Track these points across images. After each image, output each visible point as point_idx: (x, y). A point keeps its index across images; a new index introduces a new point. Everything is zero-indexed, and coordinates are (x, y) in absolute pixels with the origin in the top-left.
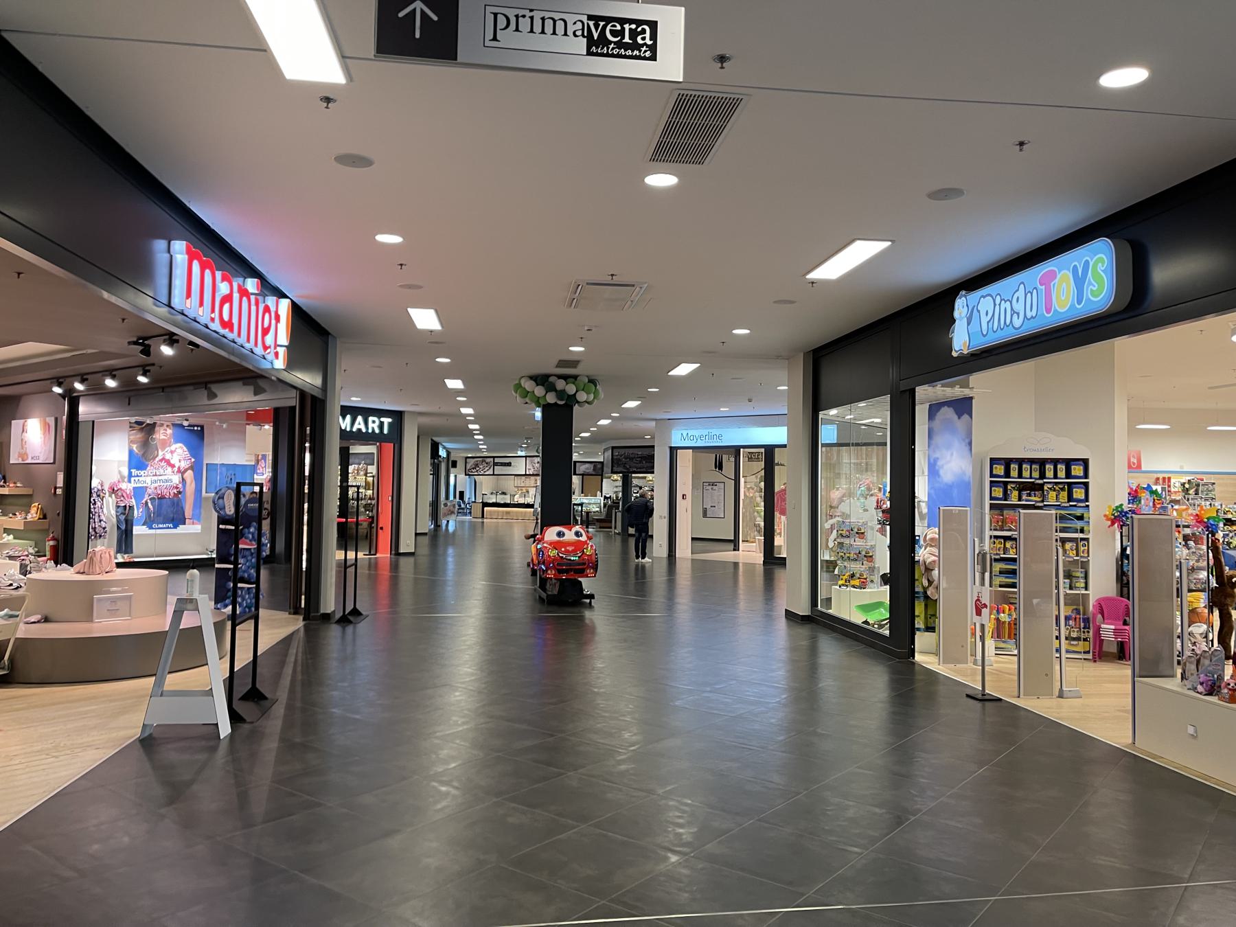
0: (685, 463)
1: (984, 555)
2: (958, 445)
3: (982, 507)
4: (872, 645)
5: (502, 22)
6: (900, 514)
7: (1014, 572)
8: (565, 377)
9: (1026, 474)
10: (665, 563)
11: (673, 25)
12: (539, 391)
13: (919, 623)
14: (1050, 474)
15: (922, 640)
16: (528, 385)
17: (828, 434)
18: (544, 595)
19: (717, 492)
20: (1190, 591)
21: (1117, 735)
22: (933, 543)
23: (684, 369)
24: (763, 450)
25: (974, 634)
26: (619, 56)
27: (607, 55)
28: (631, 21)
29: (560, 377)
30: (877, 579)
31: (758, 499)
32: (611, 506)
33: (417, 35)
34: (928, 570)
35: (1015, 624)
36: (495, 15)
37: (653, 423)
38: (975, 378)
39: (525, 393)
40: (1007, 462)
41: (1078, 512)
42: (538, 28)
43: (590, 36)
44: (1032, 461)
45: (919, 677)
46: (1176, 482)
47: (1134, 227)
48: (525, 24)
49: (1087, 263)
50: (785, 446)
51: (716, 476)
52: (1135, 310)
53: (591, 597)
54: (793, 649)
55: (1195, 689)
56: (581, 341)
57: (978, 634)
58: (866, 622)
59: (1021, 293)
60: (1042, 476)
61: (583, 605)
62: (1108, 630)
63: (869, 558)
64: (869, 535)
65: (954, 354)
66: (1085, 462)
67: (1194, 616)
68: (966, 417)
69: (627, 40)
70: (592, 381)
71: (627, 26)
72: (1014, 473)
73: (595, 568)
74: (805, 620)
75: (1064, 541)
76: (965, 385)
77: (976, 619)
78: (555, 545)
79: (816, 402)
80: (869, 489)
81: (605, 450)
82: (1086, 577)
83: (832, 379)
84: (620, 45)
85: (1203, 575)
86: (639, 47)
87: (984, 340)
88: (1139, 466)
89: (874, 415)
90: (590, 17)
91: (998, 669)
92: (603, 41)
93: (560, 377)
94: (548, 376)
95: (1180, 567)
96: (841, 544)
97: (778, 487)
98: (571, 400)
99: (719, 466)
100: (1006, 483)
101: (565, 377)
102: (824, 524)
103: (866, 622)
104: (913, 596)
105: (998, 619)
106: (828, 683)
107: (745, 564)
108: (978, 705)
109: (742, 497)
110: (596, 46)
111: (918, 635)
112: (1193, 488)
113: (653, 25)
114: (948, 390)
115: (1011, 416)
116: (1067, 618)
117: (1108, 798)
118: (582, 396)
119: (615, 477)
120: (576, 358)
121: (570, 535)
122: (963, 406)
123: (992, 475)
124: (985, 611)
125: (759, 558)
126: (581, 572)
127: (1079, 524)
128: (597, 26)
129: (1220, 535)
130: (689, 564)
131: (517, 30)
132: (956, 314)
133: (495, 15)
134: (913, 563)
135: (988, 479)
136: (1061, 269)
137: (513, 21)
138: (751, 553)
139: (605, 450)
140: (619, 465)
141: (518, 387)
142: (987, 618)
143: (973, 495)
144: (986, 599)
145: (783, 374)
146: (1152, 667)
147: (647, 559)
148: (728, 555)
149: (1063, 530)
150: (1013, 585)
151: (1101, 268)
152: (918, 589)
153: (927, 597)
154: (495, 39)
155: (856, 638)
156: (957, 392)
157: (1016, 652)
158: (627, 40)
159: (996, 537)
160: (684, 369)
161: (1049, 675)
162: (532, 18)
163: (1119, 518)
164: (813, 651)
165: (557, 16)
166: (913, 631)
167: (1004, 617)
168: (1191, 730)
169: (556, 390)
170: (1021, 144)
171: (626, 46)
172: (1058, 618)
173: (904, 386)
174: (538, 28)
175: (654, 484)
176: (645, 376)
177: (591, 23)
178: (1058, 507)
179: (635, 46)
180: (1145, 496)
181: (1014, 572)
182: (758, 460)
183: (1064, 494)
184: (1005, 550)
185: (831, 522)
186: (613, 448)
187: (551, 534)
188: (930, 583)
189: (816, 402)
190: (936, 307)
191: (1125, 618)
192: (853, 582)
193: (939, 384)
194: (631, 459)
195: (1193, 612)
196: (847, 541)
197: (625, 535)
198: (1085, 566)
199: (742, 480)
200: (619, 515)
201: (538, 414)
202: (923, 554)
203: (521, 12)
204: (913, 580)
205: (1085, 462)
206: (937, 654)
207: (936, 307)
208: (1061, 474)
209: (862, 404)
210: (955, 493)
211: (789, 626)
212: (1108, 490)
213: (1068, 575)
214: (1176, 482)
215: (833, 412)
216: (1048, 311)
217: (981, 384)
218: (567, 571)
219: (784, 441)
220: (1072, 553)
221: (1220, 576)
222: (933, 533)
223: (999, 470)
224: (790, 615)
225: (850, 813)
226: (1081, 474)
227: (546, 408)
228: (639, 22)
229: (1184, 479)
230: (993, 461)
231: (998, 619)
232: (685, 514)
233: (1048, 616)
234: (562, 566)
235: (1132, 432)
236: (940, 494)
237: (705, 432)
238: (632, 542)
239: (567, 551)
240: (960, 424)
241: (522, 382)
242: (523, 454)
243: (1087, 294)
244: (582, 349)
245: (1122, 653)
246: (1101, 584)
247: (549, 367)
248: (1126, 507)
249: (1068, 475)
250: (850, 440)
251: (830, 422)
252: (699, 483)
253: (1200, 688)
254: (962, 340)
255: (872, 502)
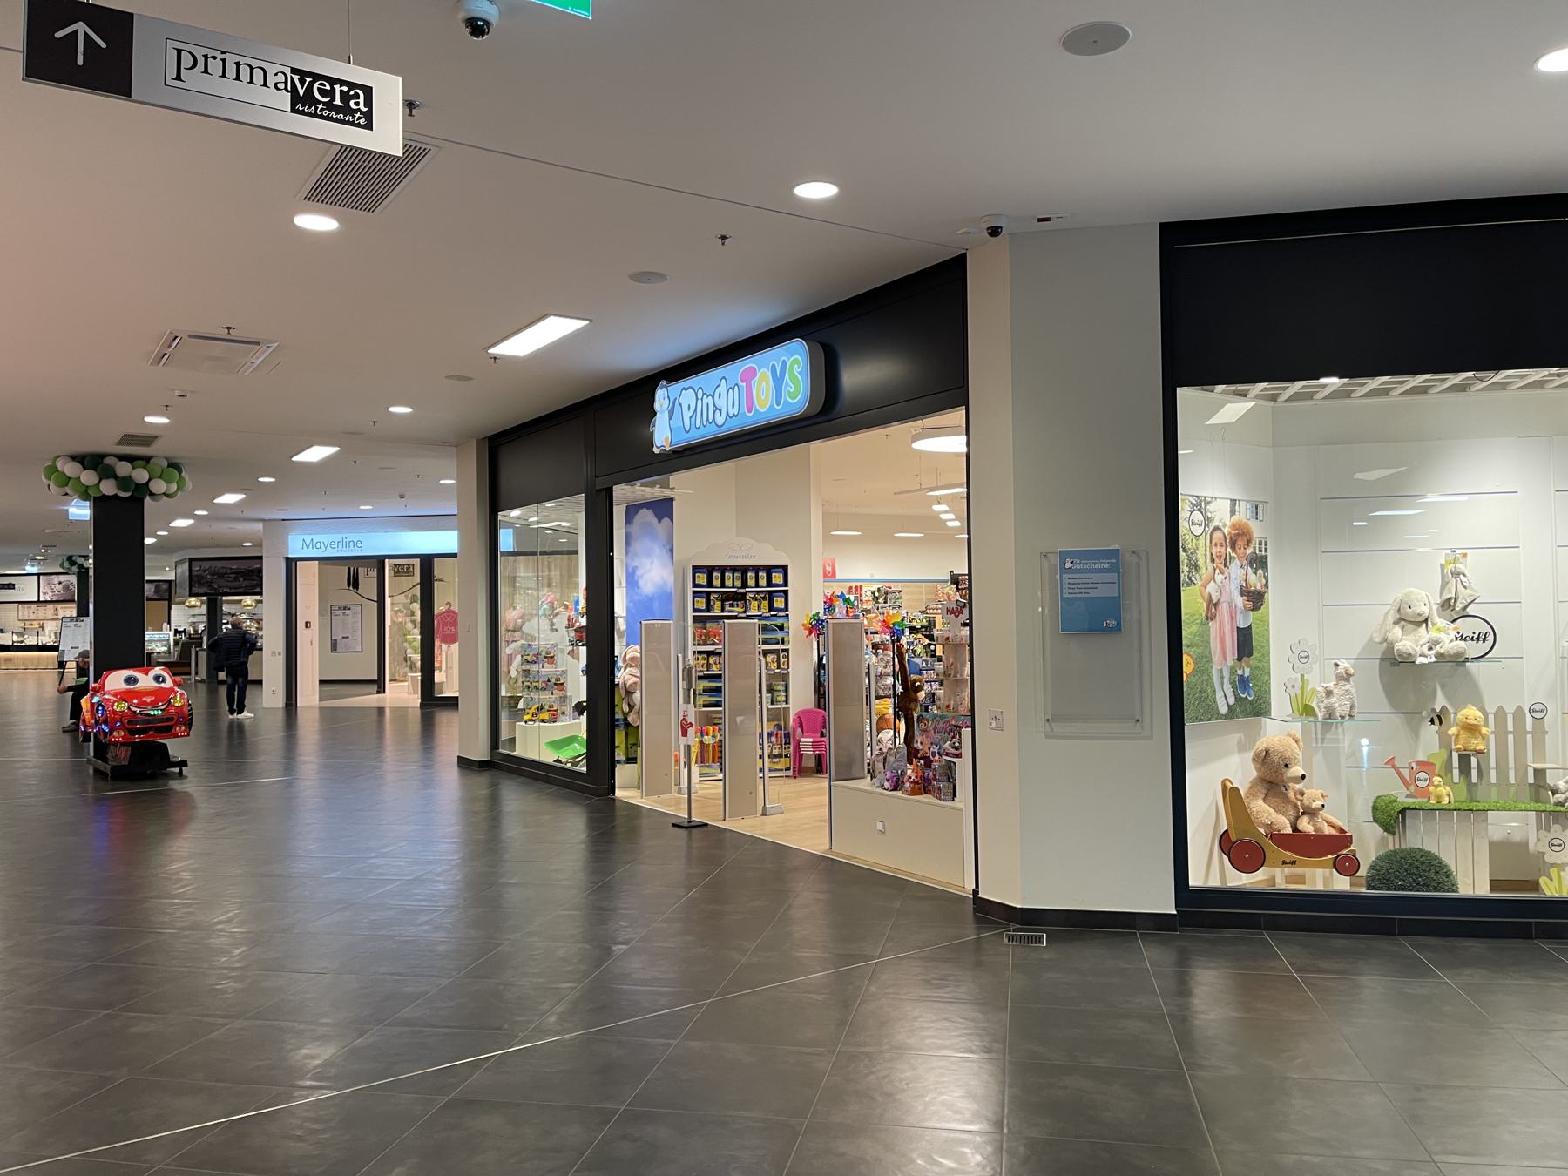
0: (308, 578)
1: (690, 670)
2: (658, 551)
3: (685, 619)
4: (566, 786)
5: (187, 61)
6: (598, 634)
7: (718, 690)
8: (131, 459)
9: (728, 583)
10: (281, 716)
11: (389, 92)
12: (89, 477)
13: (620, 755)
14: (751, 582)
15: (623, 773)
16: (71, 469)
17: (506, 541)
18: (107, 768)
19: (352, 617)
20: (878, 697)
21: (815, 843)
22: (633, 662)
23: (316, 454)
24: (417, 562)
25: (678, 761)
26: (328, 118)
27: (315, 115)
28: (342, 83)
29: (122, 458)
30: (569, 709)
31: (410, 625)
32: (186, 644)
33: (80, 62)
34: (629, 693)
35: (720, 745)
36: (179, 51)
37: (260, 526)
38: (675, 478)
39: (65, 481)
40: (710, 570)
41: (779, 622)
42: (231, 72)
43: (294, 91)
44: (734, 569)
45: (619, 813)
46: (867, 590)
47: (828, 327)
48: (216, 66)
49: (784, 363)
50: (455, 555)
51: (350, 596)
52: (829, 414)
53: (184, 763)
54: (468, 800)
55: (882, 786)
56: (165, 409)
57: (683, 760)
58: (558, 761)
59: (722, 389)
60: (745, 585)
61: (171, 776)
62: (806, 742)
63: (560, 685)
64: (559, 658)
65: (656, 451)
66: (785, 569)
67: (882, 724)
68: (666, 520)
69: (338, 102)
70: (175, 465)
71: (337, 87)
72: (717, 582)
73: (188, 723)
74: (484, 766)
75: (766, 653)
76: (666, 485)
77: (683, 741)
78: (124, 696)
79: (494, 501)
80: (553, 608)
81: (178, 563)
82: (786, 690)
83: (514, 471)
84: (330, 106)
85: (890, 680)
86: (352, 112)
87: (690, 435)
88: (834, 575)
89: (564, 517)
90: (294, 71)
91: (703, 795)
92: (309, 99)
93: (122, 458)
94: (103, 456)
95: (868, 674)
96: (527, 672)
97: (439, 608)
98: (141, 492)
99: (354, 582)
100: (709, 593)
101: (131, 459)
102: (506, 651)
103: (558, 761)
104: (613, 724)
105: (702, 743)
106: (513, 830)
107: (394, 710)
108: (683, 833)
109: (388, 622)
110: (301, 103)
111: (618, 768)
112: (883, 596)
113: (368, 91)
114: (648, 489)
115: (712, 520)
116: (770, 735)
117: (807, 898)
118: (159, 486)
119: (193, 601)
120: (154, 433)
121: (145, 681)
122: (663, 508)
123: (695, 585)
124: (691, 731)
125: (416, 700)
126: (167, 731)
127: (779, 635)
128: (302, 82)
129: (904, 640)
130: (317, 714)
131: (206, 71)
132: (657, 406)
133: (179, 51)
134: (613, 686)
135: (690, 589)
136: (761, 364)
137: (201, 61)
138: (403, 694)
139: (178, 563)
140: (200, 584)
141: (52, 470)
142: (693, 738)
143: (675, 607)
144: (691, 719)
145: (452, 465)
146: (846, 773)
147: (246, 714)
148: (371, 699)
149: (766, 642)
150: (718, 704)
151: (797, 369)
152: (619, 716)
153: (627, 724)
154: (178, 78)
155: (548, 780)
156: (657, 492)
157: (721, 776)
158: (338, 102)
159: (700, 653)
160: (316, 454)
161: (753, 793)
162: (224, 61)
163: (817, 627)
164: (494, 800)
165: (254, 63)
166: (613, 764)
167: (708, 739)
168: (880, 826)
169: (116, 477)
170: (723, 238)
171: (337, 109)
172: (761, 735)
173: (601, 483)
174: (231, 72)
175: (260, 614)
176: (256, 459)
177: (296, 78)
178: (760, 617)
179: (347, 110)
180: (839, 603)
181: (718, 690)
182: (409, 574)
183: (766, 603)
184: (709, 666)
185: (513, 645)
186: (191, 560)
187: (116, 680)
188: (631, 707)
189: (494, 501)
190: (633, 396)
191: (821, 729)
192: (542, 716)
193: (638, 483)
194: (221, 576)
195: (882, 718)
196: (534, 668)
197: (212, 681)
198: (785, 677)
199: (388, 601)
200: (203, 656)
201: (81, 511)
202: (623, 676)
203: (211, 53)
204: (613, 706)
205: (785, 569)
206: (639, 787)
207: (633, 396)
208: (763, 582)
209: (550, 504)
210: (656, 605)
211: (462, 775)
212: (806, 600)
213: (770, 690)
214: (867, 590)
215: (515, 513)
216: (750, 410)
217: (682, 485)
218: (139, 732)
219: (454, 548)
220: (773, 666)
221: (904, 683)
222: (634, 651)
223: (702, 579)
224: (464, 763)
225: (561, 953)
226: (781, 581)
227: (102, 504)
228: (352, 85)
229: (875, 588)
230: (696, 569)
231: (702, 743)
232: (303, 649)
233: (751, 735)
234: (133, 724)
235: (827, 537)
236: (641, 607)
237: (338, 537)
238: (223, 691)
239: (145, 703)
240: (661, 528)
241: (60, 464)
242: (35, 570)
243: (785, 396)
244: (165, 421)
245: (819, 768)
246: (800, 697)
247: (105, 442)
248: (822, 617)
249: (769, 584)
250: (534, 549)
251: (509, 525)
252: (331, 609)
253: (887, 785)
254: (663, 435)
255: (561, 622)
